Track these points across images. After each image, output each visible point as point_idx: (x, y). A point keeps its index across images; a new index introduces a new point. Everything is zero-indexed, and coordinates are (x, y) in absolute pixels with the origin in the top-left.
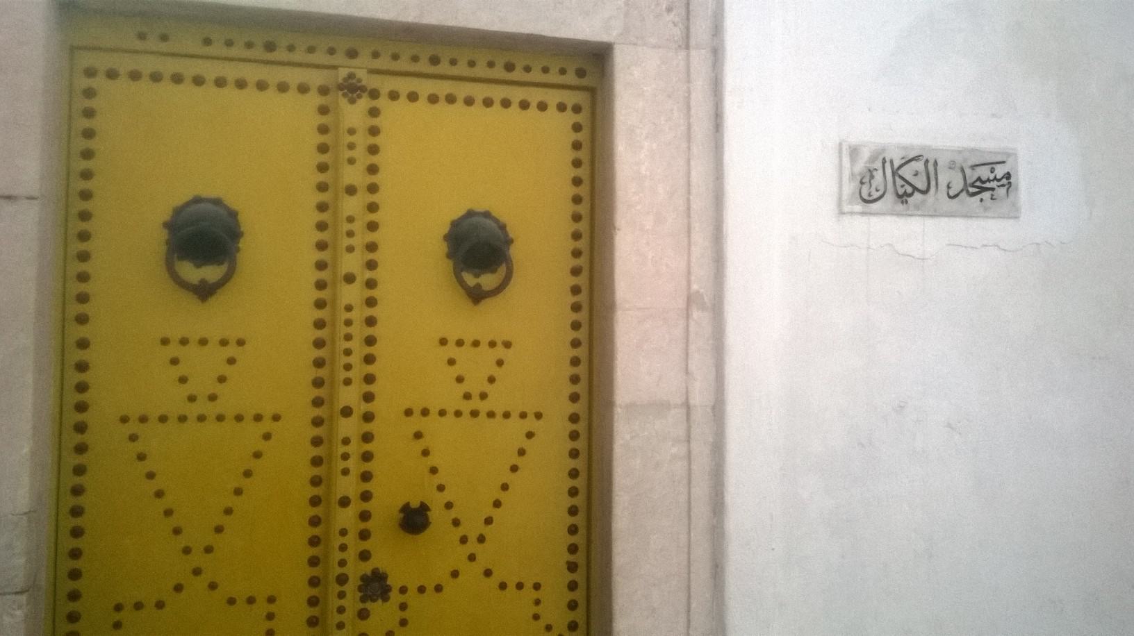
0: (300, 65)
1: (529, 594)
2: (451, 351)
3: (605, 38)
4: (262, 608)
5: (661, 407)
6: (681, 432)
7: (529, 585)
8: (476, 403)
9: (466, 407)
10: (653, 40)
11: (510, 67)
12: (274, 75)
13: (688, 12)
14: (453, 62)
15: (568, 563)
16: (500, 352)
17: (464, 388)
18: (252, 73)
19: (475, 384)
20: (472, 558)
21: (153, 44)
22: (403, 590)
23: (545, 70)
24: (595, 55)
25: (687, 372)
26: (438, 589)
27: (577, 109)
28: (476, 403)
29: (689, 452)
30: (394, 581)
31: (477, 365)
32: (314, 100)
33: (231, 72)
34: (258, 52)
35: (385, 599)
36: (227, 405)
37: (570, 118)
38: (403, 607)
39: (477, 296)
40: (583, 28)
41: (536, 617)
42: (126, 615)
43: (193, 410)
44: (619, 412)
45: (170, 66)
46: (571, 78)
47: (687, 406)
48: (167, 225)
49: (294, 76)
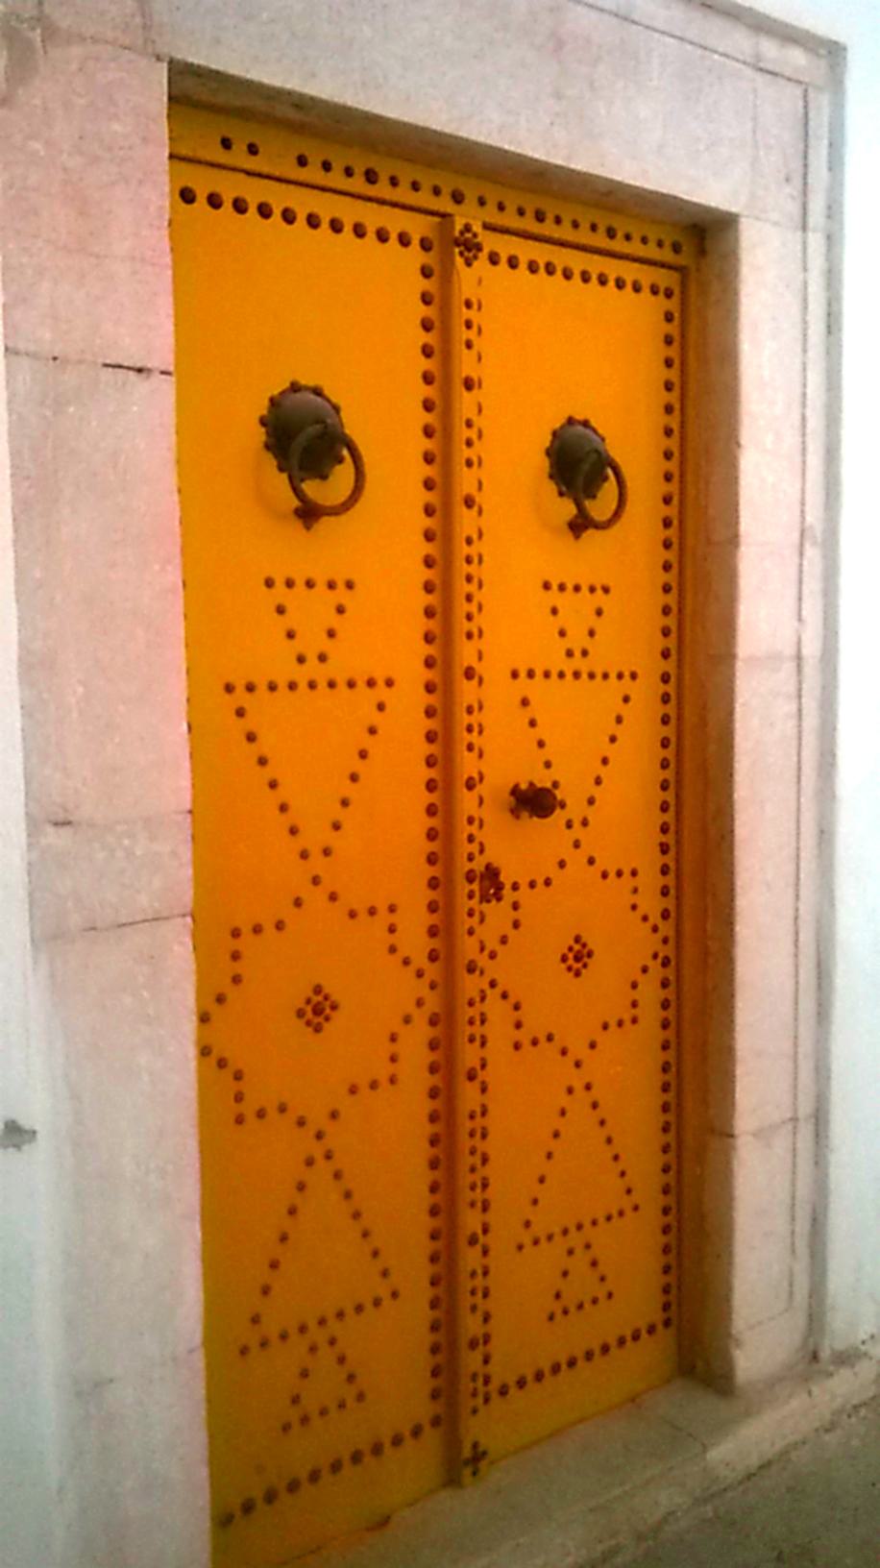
0: (382, 202)
1: (384, 918)
2: (554, 597)
3: (734, 210)
4: (384, 918)
5: (775, 658)
6: (792, 688)
7: (382, 909)
8: (577, 662)
9: (569, 667)
10: (775, 216)
11: (371, 177)
12: (374, 217)
13: (805, 184)
14: (349, 172)
15: (662, 845)
16: (341, 595)
17: (566, 643)
18: (350, 212)
19: (312, 641)
20: (577, 845)
21: (239, 157)
22: (515, 887)
23: (415, 186)
24: (695, 226)
25: (800, 619)
26: (548, 882)
27: (669, 294)
28: (577, 662)
29: (800, 710)
30: (506, 878)
31: (312, 612)
32: (415, 256)
33: (327, 207)
34: (357, 184)
35: (499, 899)
36: (337, 669)
37: (662, 303)
38: (515, 906)
39: (309, 514)
40: (710, 192)
41: (634, 907)
42: (247, 942)
43: (302, 675)
44: (740, 666)
45: (255, 192)
46: (666, 255)
47: (799, 658)
48: (263, 422)
49: (397, 222)
